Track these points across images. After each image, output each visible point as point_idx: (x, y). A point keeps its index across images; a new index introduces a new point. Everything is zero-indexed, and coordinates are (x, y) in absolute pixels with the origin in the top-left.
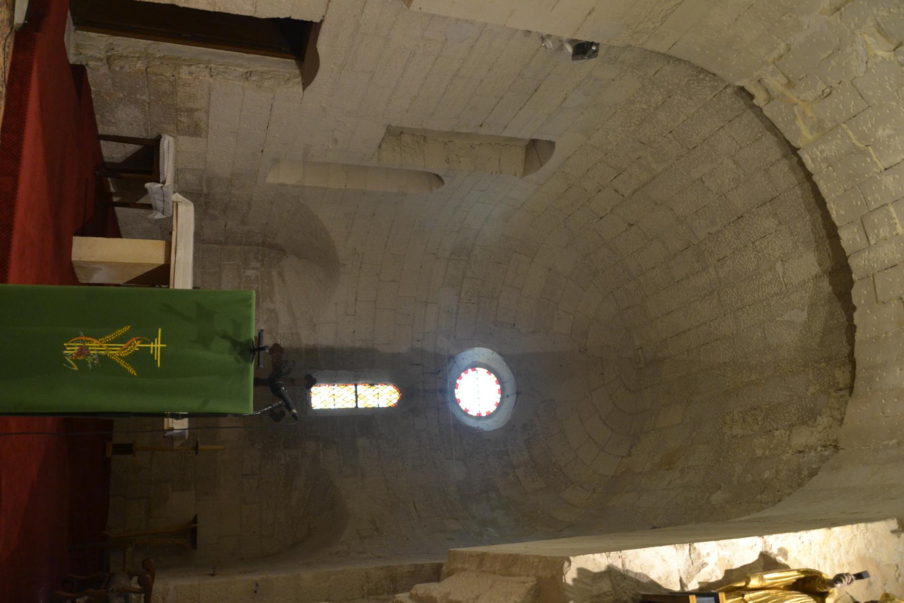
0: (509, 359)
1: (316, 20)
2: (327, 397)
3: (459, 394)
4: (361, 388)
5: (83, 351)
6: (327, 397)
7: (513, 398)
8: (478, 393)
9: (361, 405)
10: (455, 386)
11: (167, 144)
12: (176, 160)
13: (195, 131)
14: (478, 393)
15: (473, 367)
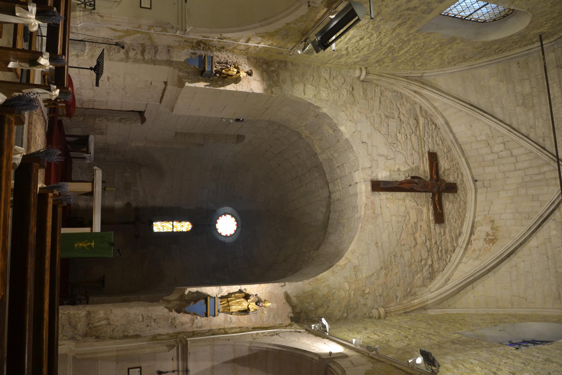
0: (238, 212)
1: (143, 110)
2: (159, 227)
3: (218, 226)
4: (175, 223)
5: (78, 245)
6: (159, 227)
7: (240, 228)
8: (226, 225)
9: (175, 230)
10: (216, 223)
11: (91, 138)
12: (95, 145)
13: (102, 134)
14: (226, 225)
15: (225, 214)
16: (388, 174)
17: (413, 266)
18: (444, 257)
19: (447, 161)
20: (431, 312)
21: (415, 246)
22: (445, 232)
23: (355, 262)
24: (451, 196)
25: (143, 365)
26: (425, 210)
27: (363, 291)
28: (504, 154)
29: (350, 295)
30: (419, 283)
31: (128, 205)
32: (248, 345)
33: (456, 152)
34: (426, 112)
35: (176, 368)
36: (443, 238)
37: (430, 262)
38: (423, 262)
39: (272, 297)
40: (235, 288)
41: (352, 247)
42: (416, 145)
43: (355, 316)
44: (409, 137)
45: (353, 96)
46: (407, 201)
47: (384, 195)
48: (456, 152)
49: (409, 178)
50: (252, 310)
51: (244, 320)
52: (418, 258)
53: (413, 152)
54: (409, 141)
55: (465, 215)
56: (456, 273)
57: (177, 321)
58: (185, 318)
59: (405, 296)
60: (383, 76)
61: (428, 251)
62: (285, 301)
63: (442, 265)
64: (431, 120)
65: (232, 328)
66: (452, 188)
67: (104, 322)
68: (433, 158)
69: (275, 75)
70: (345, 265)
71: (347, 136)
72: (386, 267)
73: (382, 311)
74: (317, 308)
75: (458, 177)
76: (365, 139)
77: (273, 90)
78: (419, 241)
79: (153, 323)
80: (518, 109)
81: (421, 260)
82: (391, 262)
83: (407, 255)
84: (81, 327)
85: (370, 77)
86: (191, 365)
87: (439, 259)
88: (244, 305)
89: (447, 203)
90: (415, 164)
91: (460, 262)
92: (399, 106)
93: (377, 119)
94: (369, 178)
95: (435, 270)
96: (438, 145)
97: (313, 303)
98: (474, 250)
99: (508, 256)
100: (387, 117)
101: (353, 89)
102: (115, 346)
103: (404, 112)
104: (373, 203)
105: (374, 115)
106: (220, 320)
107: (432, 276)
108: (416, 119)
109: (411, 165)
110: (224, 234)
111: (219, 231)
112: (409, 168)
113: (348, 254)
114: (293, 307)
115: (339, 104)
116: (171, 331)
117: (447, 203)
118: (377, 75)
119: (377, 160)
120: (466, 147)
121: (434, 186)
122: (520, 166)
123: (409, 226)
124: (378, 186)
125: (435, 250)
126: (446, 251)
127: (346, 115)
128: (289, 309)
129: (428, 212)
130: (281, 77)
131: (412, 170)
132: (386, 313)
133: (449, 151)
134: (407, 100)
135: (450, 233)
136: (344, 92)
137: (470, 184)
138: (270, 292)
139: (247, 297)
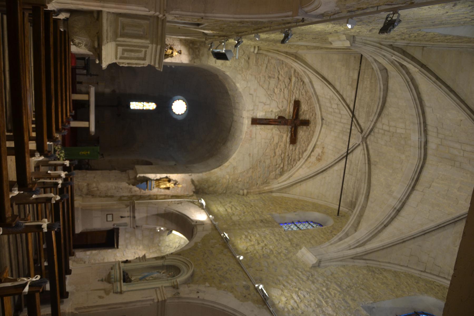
2: (134, 105)
3: (173, 107)
4: (145, 103)
6: (134, 105)
8: (179, 107)
10: (172, 105)
14: (179, 107)
16: (264, 114)
17: (271, 168)
18: (292, 163)
19: (307, 106)
20: (274, 195)
21: (274, 157)
22: (295, 149)
23: (235, 164)
24: (305, 128)
25: (114, 213)
26: (285, 136)
27: (237, 180)
28: (337, 111)
29: (229, 182)
30: (273, 177)
31: (114, 91)
32: (164, 208)
33: (314, 99)
34: (298, 74)
35: (129, 215)
36: (294, 152)
37: (282, 166)
38: (277, 166)
39: (184, 180)
40: (164, 175)
41: (234, 156)
42: (286, 96)
43: (231, 193)
44: (283, 90)
45: (248, 63)
46: (274, 130)
47: (259, 127)
48: (314, 99)
49: (277, 118)
50: (171, 188)
51: (167, 192)
52: (274, 163)
53: (284, 100)
54: (282, 93)
55: (311, 139)
56: (297, 173)
57: (133, 190)
58: (135, 188)
59: (263, 184)
60: (270, 51)
61: (282, 160)
62: (191, 183)
63: (289, 168)
64: (301, 78)
65: (161, 195)
66: (306, 123)
67: (96, 189)
68: (297, 104)
69: (197, 51)
70: (228, 166)
71: (240, 90)
72: (253, 168)
73: (245, 191)
74: (209, 187)
75: (312, 115)
76: (252, 92)
77: (195, 61)
78: (277, 154)
79: (120, 190)
80: (348, 87)
81: (277, 165)
82: (257, 166)
83: (268, 162)
84: (85, 190)
85: (261, 52)
86: (137, 215)
87: (288, 164)
88: (168, 185)
89: (301, 132)
90: (284, 108)
91: (301, 167)
92: (279, 69)
93: (262, 79)
94: (251, 116)
95: (285, 170)
96: (303, 95)
97: (207, 185)
98: (310, 162)
99: (322, 172)
100: (270, 77)
101: (249, 58)
102: (100, 203)
103: (282, 74)
104: (251, 131)
105: (261, 76)
106: (155, 191)
107: (281, 174)
108: (290, 79)
109: (281, 108)
110: (177, 113)
111: (174, 111)
112: (279, 110)
113: (231, 160)
114: (196, 186)
115: (238, 69)
116: (129, 194)
117: (301, 132)
118: (266, 50)
119: (258, 106)
120: (320, 98)
121: (295, 122)
122: (343, 121)
123: (273, 145)
124: (255, 121)
125: (286, 159)
126: (294, 160)
127: (242, 76)
128: (193, 187)
129: (286, 137)
130: (201, 52)
131: (281, 111)
132: (248, 193)
133: (309, 99)
134: (286, 65)
135: (299, 149)
136: (243, 61)
137: (319, 121)
138: (183, 178)
139: (169, 181)
